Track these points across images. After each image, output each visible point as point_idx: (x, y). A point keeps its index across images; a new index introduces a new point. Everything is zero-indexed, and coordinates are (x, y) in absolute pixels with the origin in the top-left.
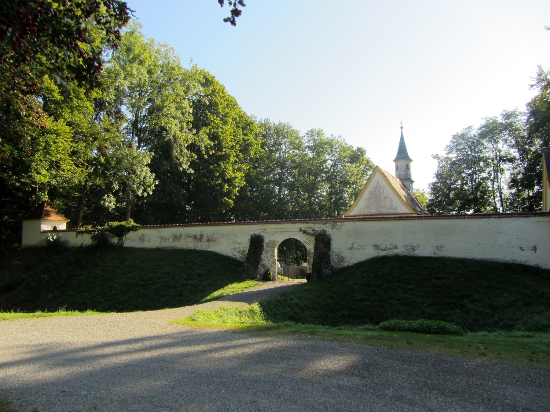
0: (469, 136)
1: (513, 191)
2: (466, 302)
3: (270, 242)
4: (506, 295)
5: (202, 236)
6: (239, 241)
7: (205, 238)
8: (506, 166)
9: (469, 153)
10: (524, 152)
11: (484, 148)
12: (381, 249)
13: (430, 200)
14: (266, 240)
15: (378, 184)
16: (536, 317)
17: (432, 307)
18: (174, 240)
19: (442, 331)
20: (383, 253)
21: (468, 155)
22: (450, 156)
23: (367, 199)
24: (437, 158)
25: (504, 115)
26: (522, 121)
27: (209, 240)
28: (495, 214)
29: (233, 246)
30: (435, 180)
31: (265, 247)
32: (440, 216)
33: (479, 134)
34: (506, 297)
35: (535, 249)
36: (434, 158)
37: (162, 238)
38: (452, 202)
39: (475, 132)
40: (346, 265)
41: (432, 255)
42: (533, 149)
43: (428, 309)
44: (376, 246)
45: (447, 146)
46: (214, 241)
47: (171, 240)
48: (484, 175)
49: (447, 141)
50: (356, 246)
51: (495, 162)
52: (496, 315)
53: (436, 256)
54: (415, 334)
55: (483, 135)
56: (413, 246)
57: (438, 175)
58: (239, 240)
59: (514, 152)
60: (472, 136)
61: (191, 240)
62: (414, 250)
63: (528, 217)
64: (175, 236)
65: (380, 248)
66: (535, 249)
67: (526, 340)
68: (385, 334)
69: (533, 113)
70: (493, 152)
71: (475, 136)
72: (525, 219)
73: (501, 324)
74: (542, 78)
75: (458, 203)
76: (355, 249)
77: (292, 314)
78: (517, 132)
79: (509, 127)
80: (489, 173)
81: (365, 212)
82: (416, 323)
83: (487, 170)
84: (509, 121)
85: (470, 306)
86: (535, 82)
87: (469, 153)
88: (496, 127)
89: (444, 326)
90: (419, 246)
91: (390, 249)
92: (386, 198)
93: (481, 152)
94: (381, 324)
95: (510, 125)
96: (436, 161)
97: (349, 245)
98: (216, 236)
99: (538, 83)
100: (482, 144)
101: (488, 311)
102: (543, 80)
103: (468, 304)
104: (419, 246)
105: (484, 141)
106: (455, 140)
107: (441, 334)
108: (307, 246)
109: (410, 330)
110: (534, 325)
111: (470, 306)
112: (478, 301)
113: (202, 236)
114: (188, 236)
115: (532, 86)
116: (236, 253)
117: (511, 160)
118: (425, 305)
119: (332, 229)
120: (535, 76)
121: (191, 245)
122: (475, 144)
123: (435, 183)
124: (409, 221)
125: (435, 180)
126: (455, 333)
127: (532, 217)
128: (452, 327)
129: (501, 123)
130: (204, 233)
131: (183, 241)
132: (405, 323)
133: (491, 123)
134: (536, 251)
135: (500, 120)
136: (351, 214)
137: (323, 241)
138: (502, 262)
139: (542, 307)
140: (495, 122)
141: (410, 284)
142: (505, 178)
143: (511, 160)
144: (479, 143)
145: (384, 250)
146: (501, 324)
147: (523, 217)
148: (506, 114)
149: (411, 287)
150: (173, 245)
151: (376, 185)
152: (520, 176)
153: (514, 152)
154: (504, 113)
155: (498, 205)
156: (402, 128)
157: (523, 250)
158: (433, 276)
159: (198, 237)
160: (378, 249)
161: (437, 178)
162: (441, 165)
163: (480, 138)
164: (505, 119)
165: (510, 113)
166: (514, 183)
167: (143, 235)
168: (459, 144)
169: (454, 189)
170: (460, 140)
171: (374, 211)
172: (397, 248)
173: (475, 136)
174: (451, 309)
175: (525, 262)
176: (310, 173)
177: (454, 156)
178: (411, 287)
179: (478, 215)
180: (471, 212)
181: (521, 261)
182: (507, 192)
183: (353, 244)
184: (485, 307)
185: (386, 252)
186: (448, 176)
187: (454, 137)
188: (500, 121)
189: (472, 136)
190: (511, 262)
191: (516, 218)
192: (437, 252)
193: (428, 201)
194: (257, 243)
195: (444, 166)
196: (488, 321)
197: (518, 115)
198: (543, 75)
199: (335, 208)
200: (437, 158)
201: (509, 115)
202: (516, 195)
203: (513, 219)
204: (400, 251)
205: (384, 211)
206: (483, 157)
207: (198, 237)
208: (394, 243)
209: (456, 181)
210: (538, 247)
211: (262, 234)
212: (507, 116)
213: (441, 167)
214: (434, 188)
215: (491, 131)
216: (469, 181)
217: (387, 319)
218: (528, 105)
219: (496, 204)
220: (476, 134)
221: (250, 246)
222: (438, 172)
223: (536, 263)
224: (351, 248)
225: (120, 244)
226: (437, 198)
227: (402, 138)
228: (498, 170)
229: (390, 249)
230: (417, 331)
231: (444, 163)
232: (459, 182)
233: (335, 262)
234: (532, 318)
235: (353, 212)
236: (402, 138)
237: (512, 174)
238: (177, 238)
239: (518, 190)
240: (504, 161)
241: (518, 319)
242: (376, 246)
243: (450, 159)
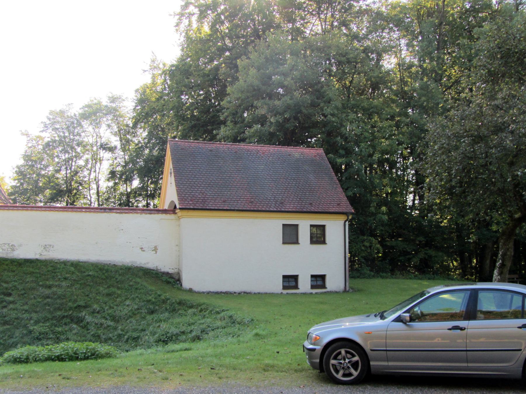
0: (69, 114)
1: (111, 184)
2: (83, 314)
4: (128, 302)
8: (106, 155)
9: (67, 134)
10: (125, 143)
11: (84, 132)
13: (12, 187)
16: (164, 326)
17: (41, 324)
19: (94, 356)
21: (65, 137)
22: (43, 135)
24: (27, 135)
25: (109, 97)
26: (128, 108)
28: (89, 209)
30: (21, 162)
32: (24, 208)
33: (79, 114)
34: (128, 305)
36: (23, 134)
38: (41, 190)
39: (76, 110)
41: (38, 257)
42: (136, 140)
43: (35, 327)
45: (42, 122)
48: (81, 162)
49: (43, 117)
51: (95, 148)
52: (120, 328)
53: (43, 258)
54: (58, 363)
55: (85, 116)
57: (27, 157)
59: (116, 141)
60: (73, 115)
62: (13, 250)
63: (151, 214)
66: (155, 249)
67: (185, 354)
68: (21, 368)
69: (141, 101)
70: (93, 137)
71: (75, 115)
72: (148, 215)
73: (126, 337)
74: (155, 65)
75: (48, 192)
78: (122, 119)
79: (113, 112)
80: (87, 161)
82: (58, 349)
83: (86, 156)
84: (114, 105)
85: (89, 319)
86: (147, 68)
87: (67, 134)
88: (99, 110)
89: (94, 349)
90: (20, 245)
93: (80, 136)
94: (6, 355)
95: (115, 110)
96: (25, 139)
99: (151, 69)
100: (82, 127)
101: (112, 323)
102: (155, 68)
103: (87, 317)
104: (20, 245)
105: (85, 124)
106: (51, 117)
107: (92, 359)
109: (50, 359)
110: (163, 335)
111: (89, 319)
112: (98, 312)
115: (145, 71)
117: (112, 149)
118: (32, 322)
120: (149, 62)
122: (74, 124)
123: (22, 166)
124: (11, 212)
125: (21, 162)
126: (108, 355)
127: (155, 214)
128: (102, 348)
129: (106, 106)
132: (41, 350)
133: (96, 104)
134: (156, 252)
135: (105, 102)
138: (121, 264)
139: (167, 314)
140: (99, 103)
141: (10, 295)
142: (105, 168)
143: (112, 149)
144: (80, 125)
146: (126, 337)
147: (146, 214)
148: (112, 97)
149: (11, 299)
152: (119, 169)
153: (116, 141)
154: (111, 96)
155: (94, 197)
157: (144, 251)
158: (41, 283)
161: (25, 160)
162: (30, 145)
163: (80, 119)
164: (111, 102)
165: (115, 96)
166: (113, 174)
168: (55, 122)
169: (44, 176)
170: (56, 118)
173: (75, 115)
174: (66, 324)
175: (145, 264)
176: (279, 54)
177: (47, 136)
178: (11, 299)
179: (71, 207)
180: (64, 204)
181: (141, 263)
182: (105, 185)
184: (107, 319)
186: (39, 159)
187: (51, 113)
188: (104, 103)
189: (73, 115)
190: (130, 265)
191: (139, 215)
192: (45, 253)
193: (9, 188)
195: (35, 147)
196: (111, 335)
197: (124, 100)
198: (156, 62)
200: (27, 135)
201: (115, 98)
202: (114, 188)
203: (135, 215)
206: (83, 142)
209: (46, 167)
210: (159, 248)
212: (113, 100)
213: (30, 147)
214: (21, 174)
215: (93, 113)
216: (63, 168)
217: (14, 346)
218: (137, 91)
219: (91, 197)
220: (77, 113)
222: (26, 152)
223: (155, 266)
226: (22, 184)
228: (96, 159)
230: (60, 359)
231: (34, 142)
232: (51, 168)
234: (159, 326)
237: (111, 165)
239: (116, 184)
240: (104, 149)
241: (143, 330)
243: (42, 138)
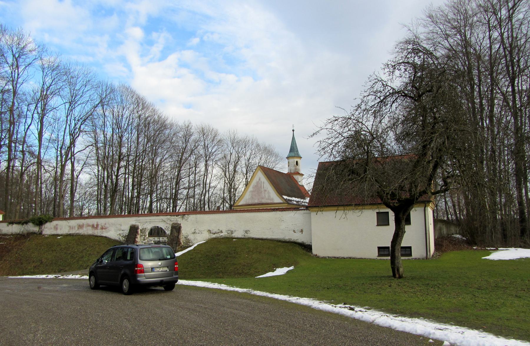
3: (143, 229)
5: (97, 225)
6: (122, 229)
7: (100, 227)
14: (140, 228)
15: (259, 179)
18: (78, 228)
20: (214, 236)
23: (251, 191)
27: (102, 228)
29: (119, 232)
35: (302, 231)
37: (70, 227)
44: (209, 231)
46: (105, 229)
47: (76, 229)
50: (197, 231)
58: (123, 228)
61: (90, 228)
62: (232, 233)
64: (79, 226)
66: (302, 231)
77: (24, 67)
81: (250, 202)
90: (235, 231)
92: (265, 191)
97: (193, 230)
98: (107, 225)
104: (235, 231)
108: (166, 231)
113: (97, 225)
114: (88, 225)
116: (120, 238)
121: (89, 231)
130: (99, 223)
131: (84, 229)
136: (240, 204)
137: (176, 228)
145: (214, 234)
150: (78, 232)
156: (293, 131)
159: (95, 226)
167: (57, 225)
171: (256, 201)
194: (134, 230)
205: (264, 201)
207: (95, 226)
208: (221, 229)
210: (304, 230)
211: (137, 224)
224: (194, 233)
225: (40, 232)
227: (293, 138)
236: (293, 138)
238: (80, 227)
242: (209, 231)
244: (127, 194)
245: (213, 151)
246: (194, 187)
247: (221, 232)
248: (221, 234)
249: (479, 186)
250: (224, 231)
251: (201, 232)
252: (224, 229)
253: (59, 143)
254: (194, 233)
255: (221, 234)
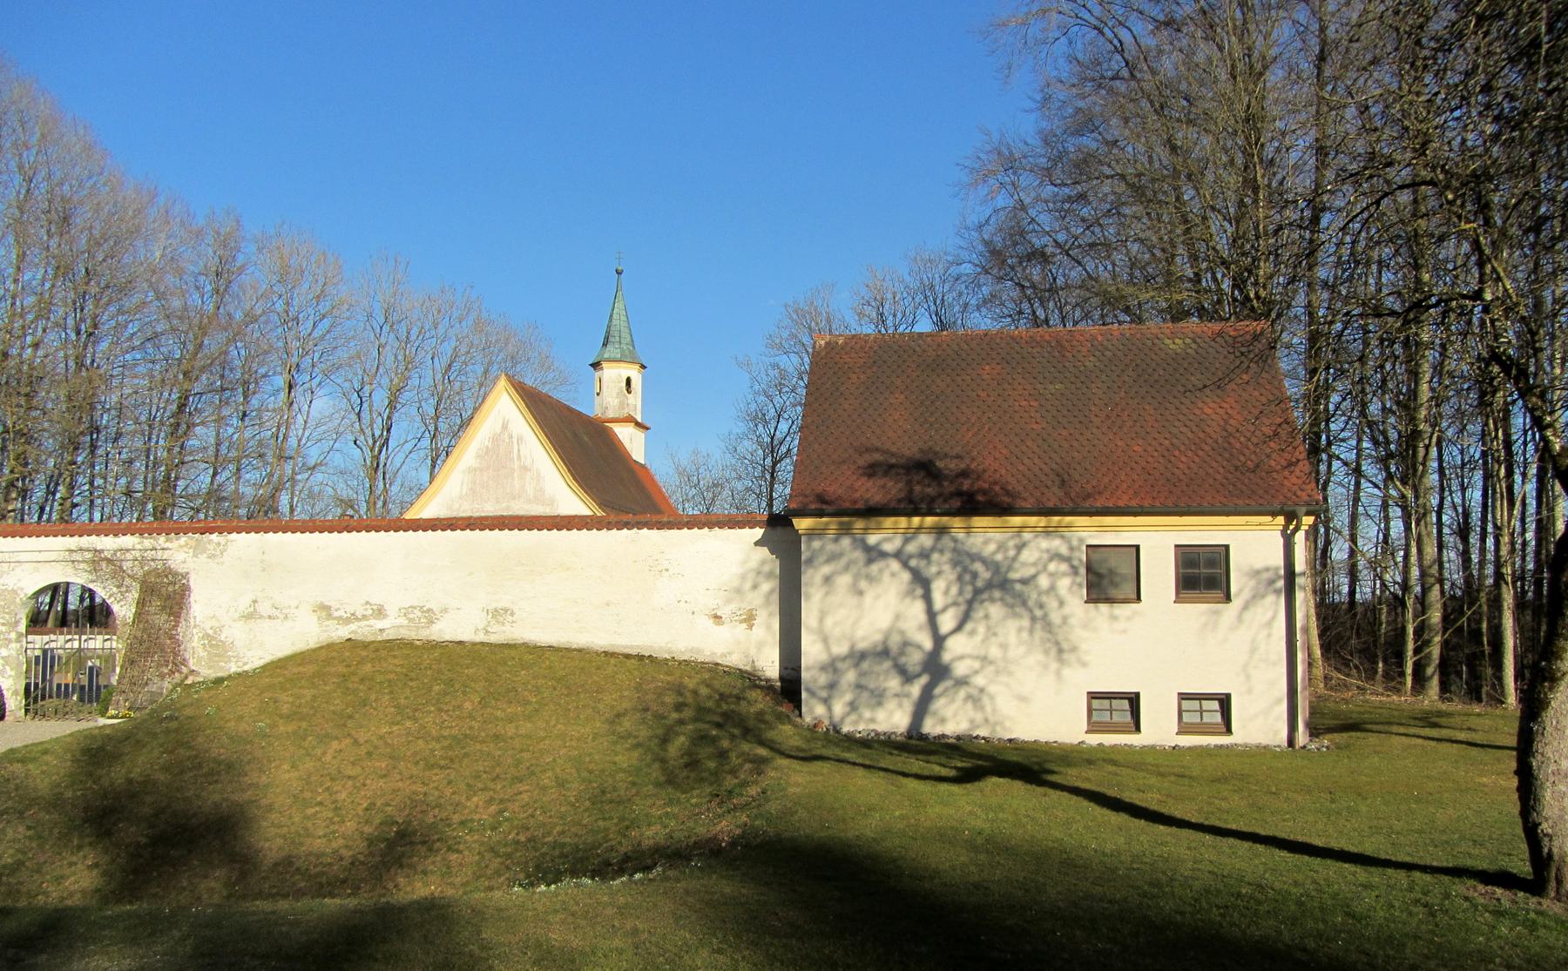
12: (340, 618)
15: (505, 427)
20: (342, 633)
23: (471, 470)
31: (1489, 888)
40: (234, 668)
44: (324, 610)
56: (429, 610)
65: (336, 614)
76: (261, 617)
91: (365, 617)
92: (525, 469)
97: (244, 604)
104: (445, 610)
119: (195, 556)
137: (166, 594)
145: (347, 621)
151: (498, 429)
160: (330, 617)
172: (385, 616)
175: (724, 655)
183: (255, 602)
185: (353, 627)
199: (979, 478)
204: (391, 626)
208: (376, 600)
221: (241, 676)
224: (249, 617)
229: (365, 617)
233: (200, 659)
235: (427, 509)
242: (324, 610)
244: (1021, 468)
245: (317, 333)
246: (1463, 464)
247: (380, 612)
248: (379, 624)
249: (1069, 199)
250: (392, 610)
251: (281, 614)
252: (394, 603)
253: (1435, 464)
254: (249, 617)
255: (379, 624)
